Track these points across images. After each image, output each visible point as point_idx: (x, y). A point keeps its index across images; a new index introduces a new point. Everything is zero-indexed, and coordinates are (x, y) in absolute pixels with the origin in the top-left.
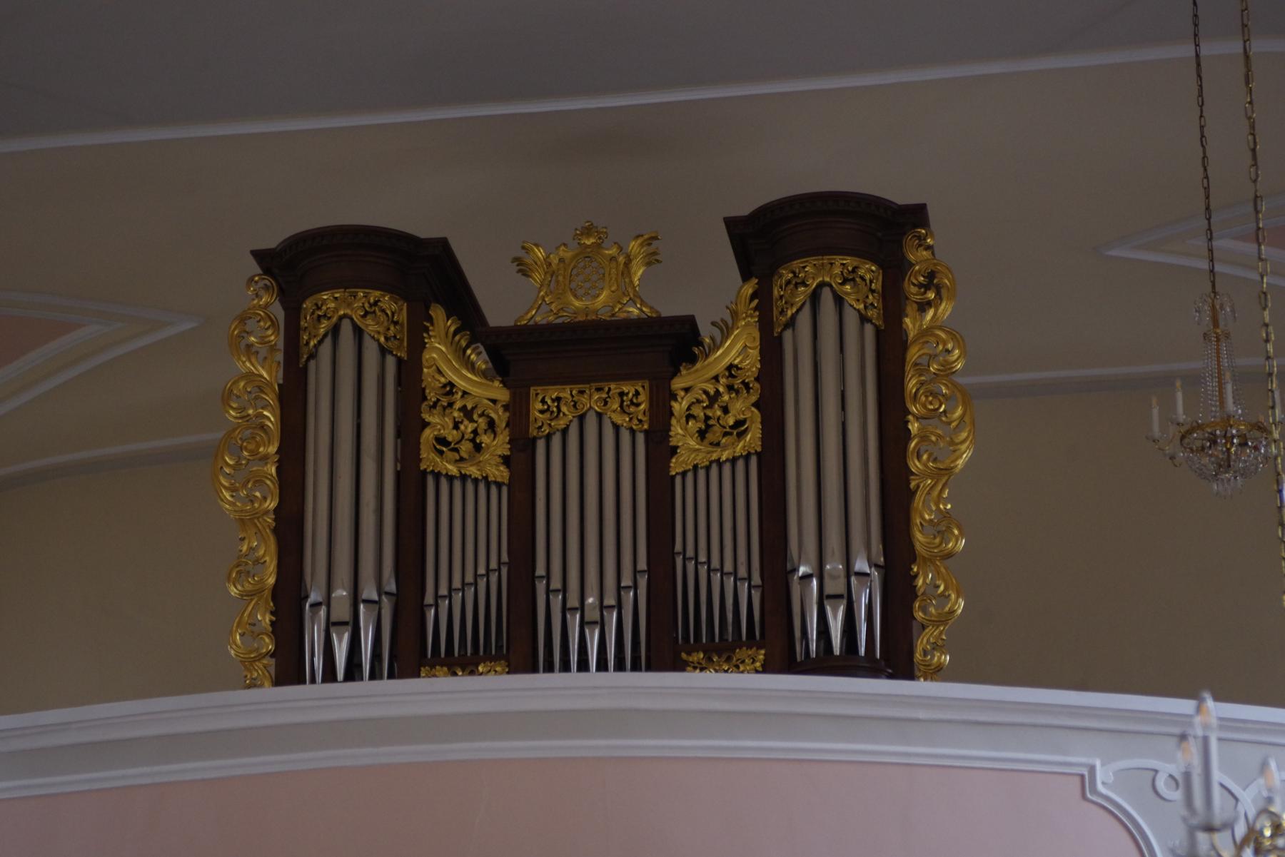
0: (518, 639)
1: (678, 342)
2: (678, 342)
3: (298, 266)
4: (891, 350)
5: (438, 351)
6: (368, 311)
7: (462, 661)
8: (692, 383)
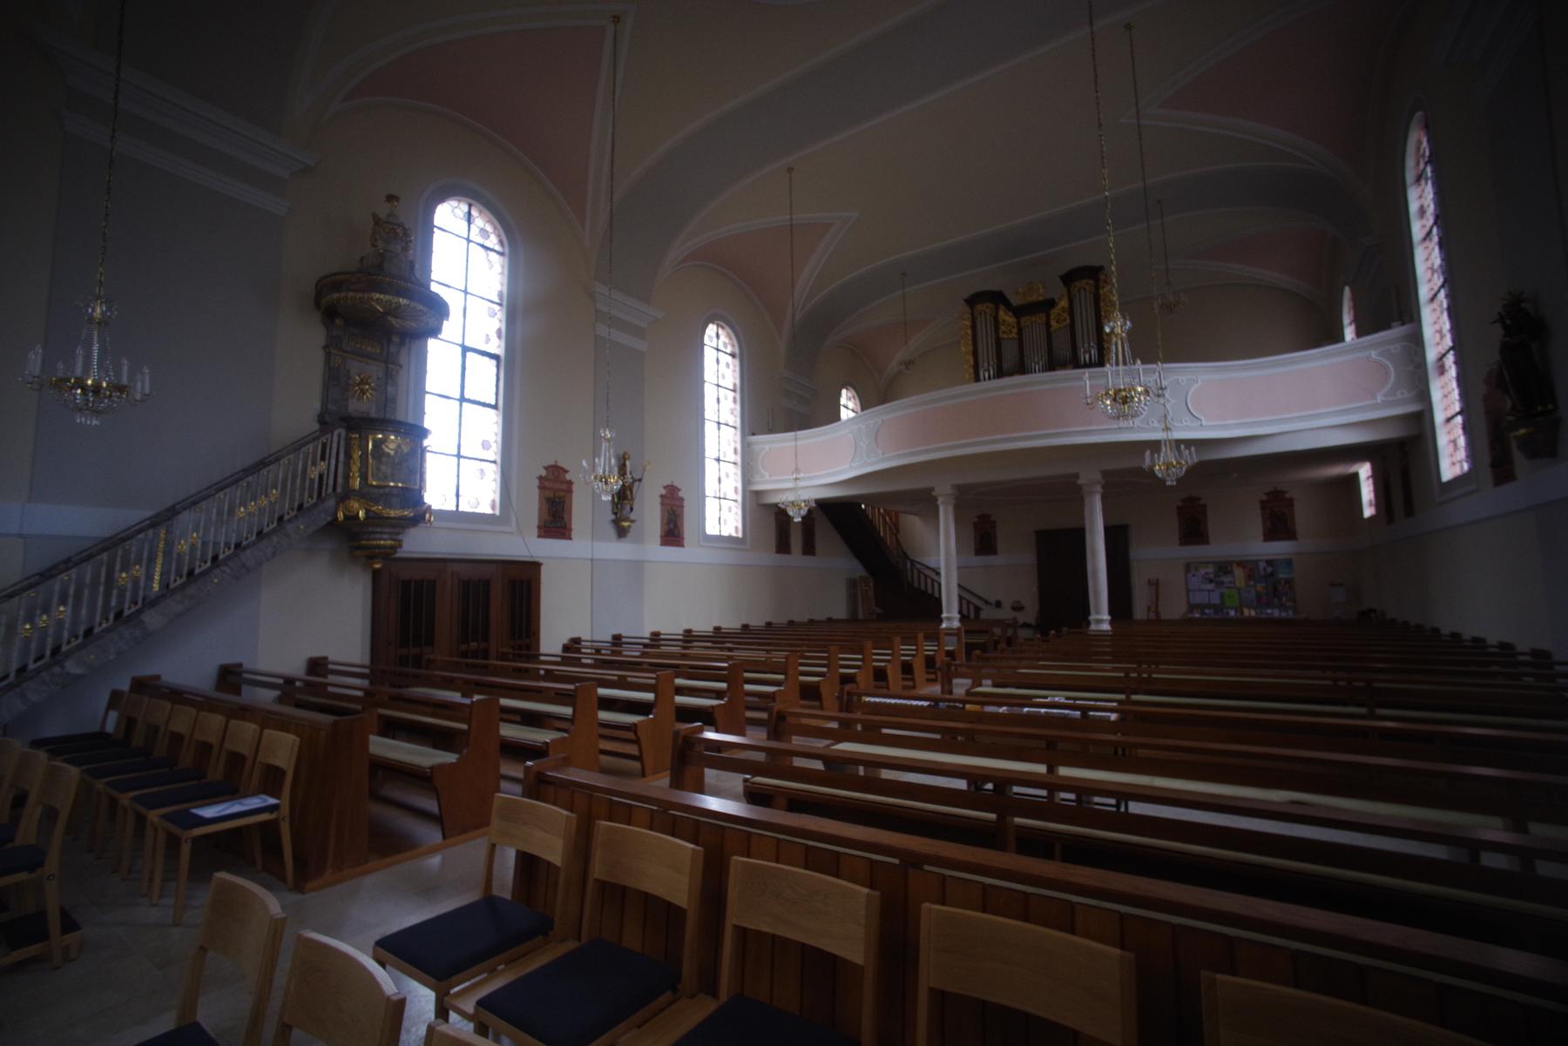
0: (1022, 369)
1: (1051, 303)
2: (1051, 303)
3: (972, 301)
4: (1097, 299)
5: (1001, 313)
6: (985, 308)
7: (1011, 374)
8: (1054, 312)
